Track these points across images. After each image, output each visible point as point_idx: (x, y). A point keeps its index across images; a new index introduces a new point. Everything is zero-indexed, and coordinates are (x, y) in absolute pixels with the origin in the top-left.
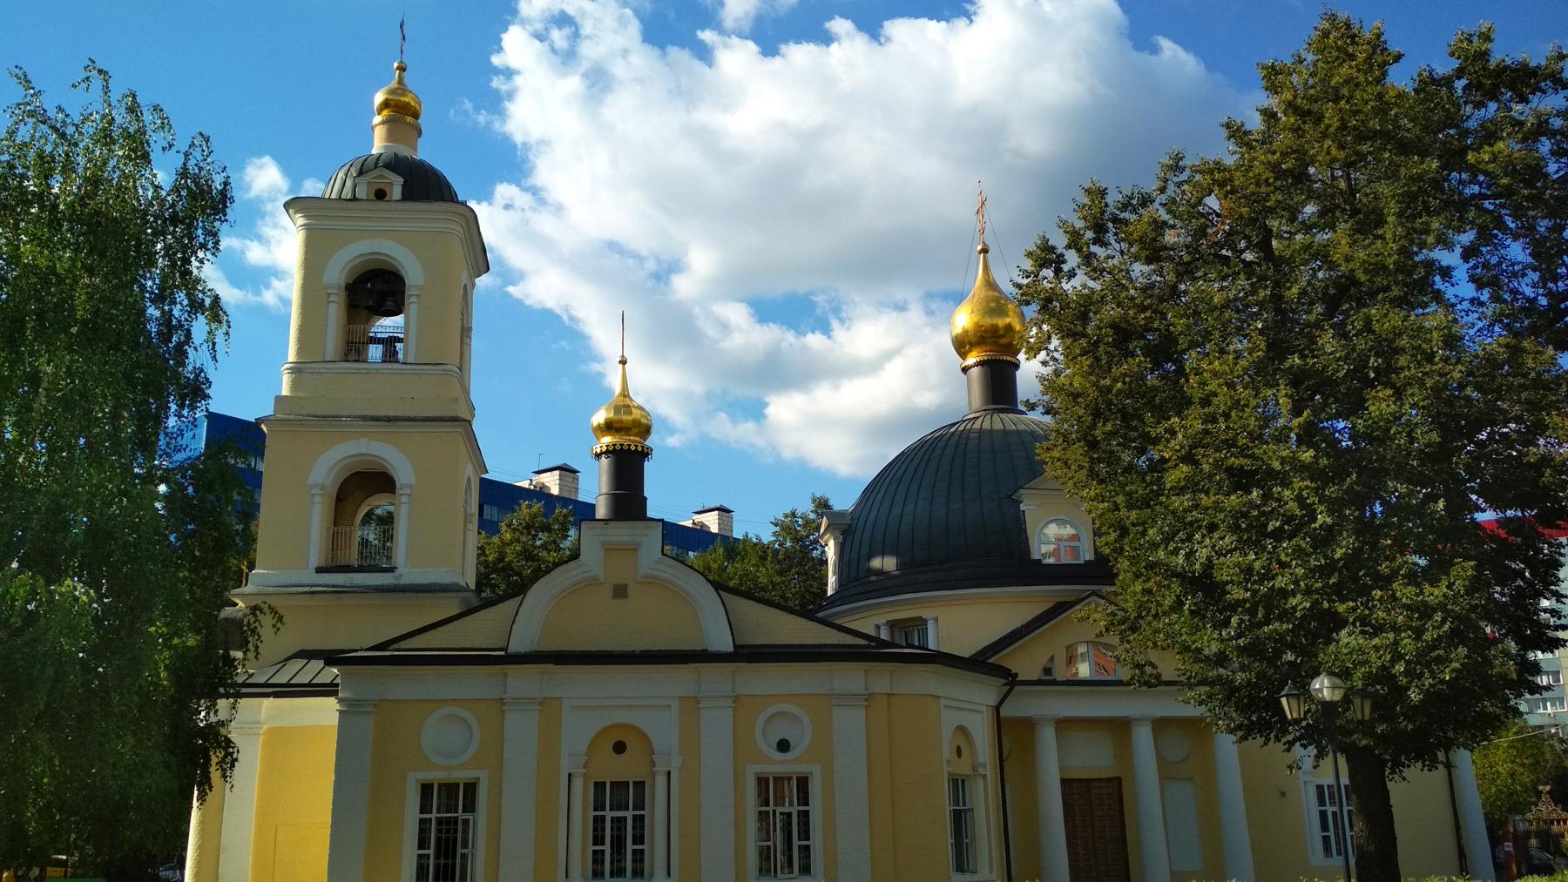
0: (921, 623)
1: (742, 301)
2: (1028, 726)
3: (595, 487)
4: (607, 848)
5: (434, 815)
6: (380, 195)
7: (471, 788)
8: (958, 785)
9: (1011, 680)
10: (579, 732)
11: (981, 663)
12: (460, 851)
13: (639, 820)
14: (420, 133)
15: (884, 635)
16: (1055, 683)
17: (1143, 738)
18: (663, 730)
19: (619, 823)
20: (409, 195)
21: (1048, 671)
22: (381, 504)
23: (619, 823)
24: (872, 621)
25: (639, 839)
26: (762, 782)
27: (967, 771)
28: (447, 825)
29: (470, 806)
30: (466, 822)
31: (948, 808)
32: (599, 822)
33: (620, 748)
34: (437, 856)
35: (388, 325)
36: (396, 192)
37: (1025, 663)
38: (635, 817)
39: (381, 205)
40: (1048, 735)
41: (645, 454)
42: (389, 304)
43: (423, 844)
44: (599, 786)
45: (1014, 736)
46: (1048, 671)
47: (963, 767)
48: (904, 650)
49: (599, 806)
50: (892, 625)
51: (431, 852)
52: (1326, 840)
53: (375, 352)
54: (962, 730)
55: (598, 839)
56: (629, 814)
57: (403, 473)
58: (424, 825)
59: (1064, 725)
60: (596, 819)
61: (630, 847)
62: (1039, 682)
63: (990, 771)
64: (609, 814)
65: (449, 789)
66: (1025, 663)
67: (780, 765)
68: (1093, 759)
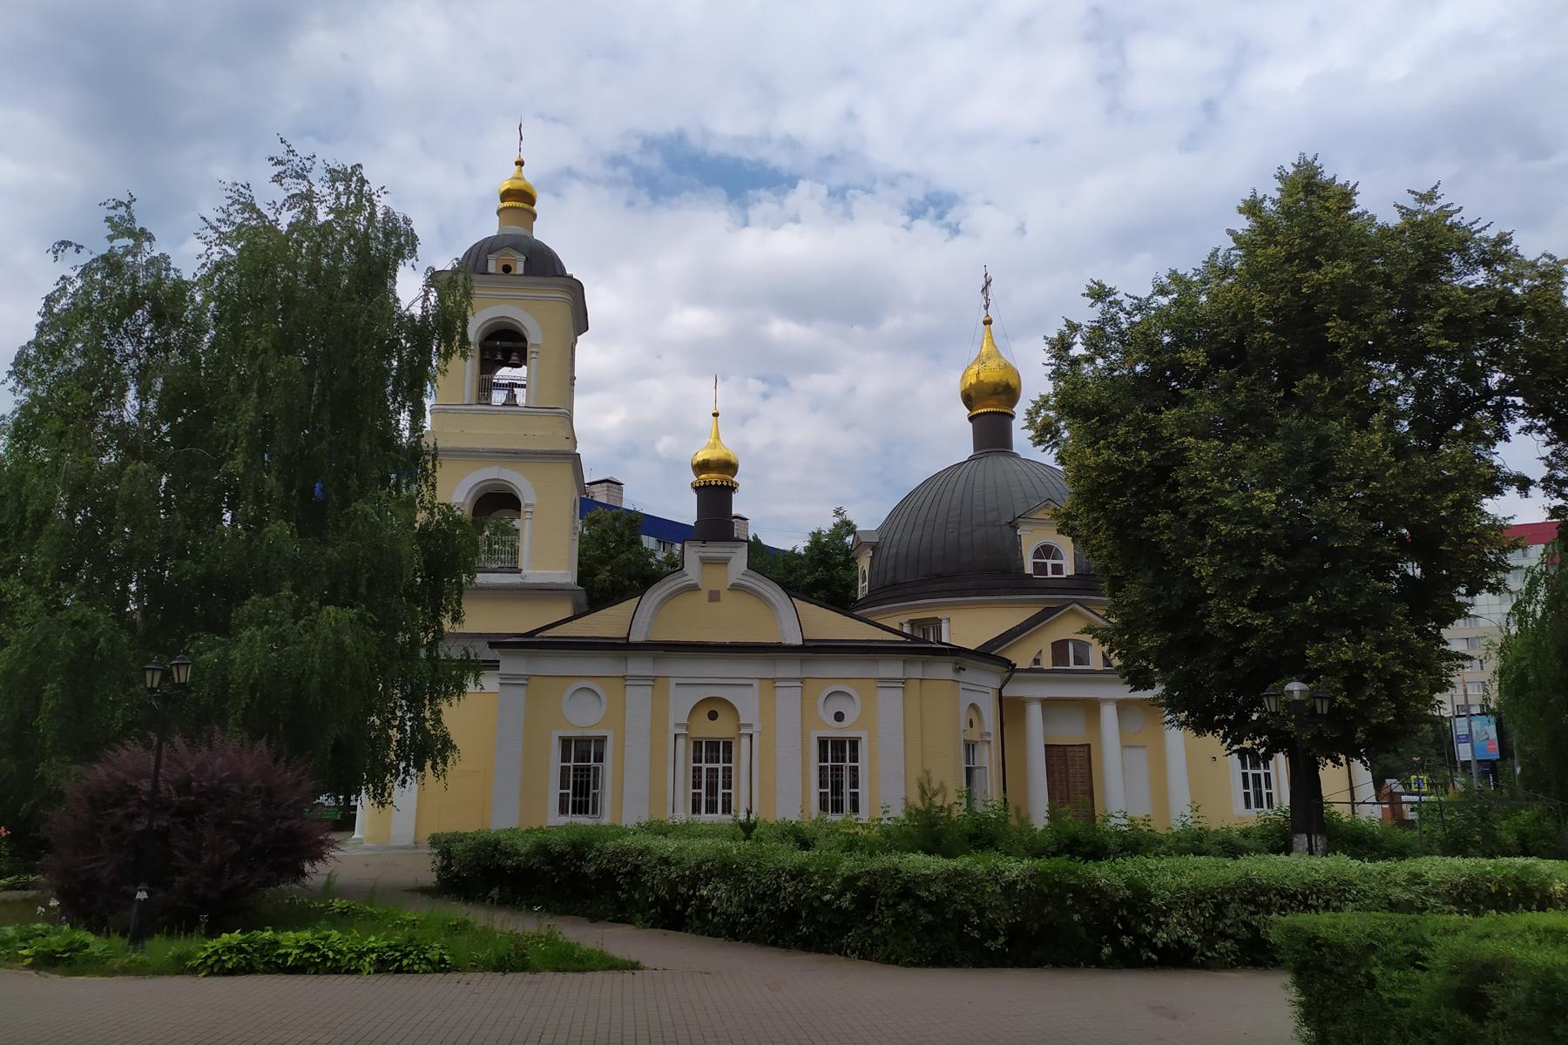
0: (936, 623)
1: (1016, 455)
2: (1020, 704)
3: (685, 511)
4: (703, 791)
5: (572, 764)
6: (507, 269)
7: (601, 741)
8: (970, 747)
9: (1011, 667)
10: (681, 703)
11: (989, 655)
12: (592, 791)
13: (727, 771)
14: (534, 216)
15: (906, 630)
16: (1042, 671)
17: (1109, 714)
18: (747, 702)
19: (712, 772)
20: (529, 271)
21: (1036, 661)
22: (504, 516)
23: (712, 772)
24: (899, 619)
25: (727, 785)
26: (823, 743)
27: (976, 738)
28: (582, 772)
29: (600, 758)
30: (596, 769)
31: (964, 766)
32: (697, 771)
33: (713, 716)
34: (575, 795)
35: (505, 374)
36: (519, 268)
37: (1021, 656)
38: (843, 760)
39: (507, 278)
40: (1035, 713)
41: (732, 488)
42: (514, 359)
43: (564, 785)
44: (697, 744)
45: (1010, 711)
46: (1036, 661)
47: (974, 735)
48: (922, 647)
49: (697, 759)
50: (912, 623)
51: (570, 791)
52: (1247, 795)
53: (499, 397)
54: (973, 706)
55: (697, 785)
56: (720, 766)
57: (527, 496)
58: (564, 771)
59: (1048, 704)
60: (695, 769)
61: (721, 791)
62: (1030, 670)
63: (995, 739)
64: (704, 766)
65: (584, 741)
66: (1021, 656)
67: (834, 731)
68: (1071, 732)
